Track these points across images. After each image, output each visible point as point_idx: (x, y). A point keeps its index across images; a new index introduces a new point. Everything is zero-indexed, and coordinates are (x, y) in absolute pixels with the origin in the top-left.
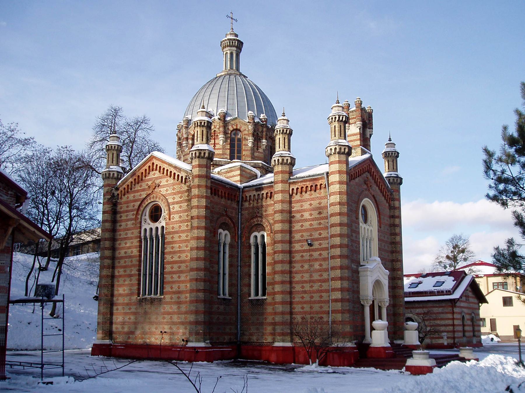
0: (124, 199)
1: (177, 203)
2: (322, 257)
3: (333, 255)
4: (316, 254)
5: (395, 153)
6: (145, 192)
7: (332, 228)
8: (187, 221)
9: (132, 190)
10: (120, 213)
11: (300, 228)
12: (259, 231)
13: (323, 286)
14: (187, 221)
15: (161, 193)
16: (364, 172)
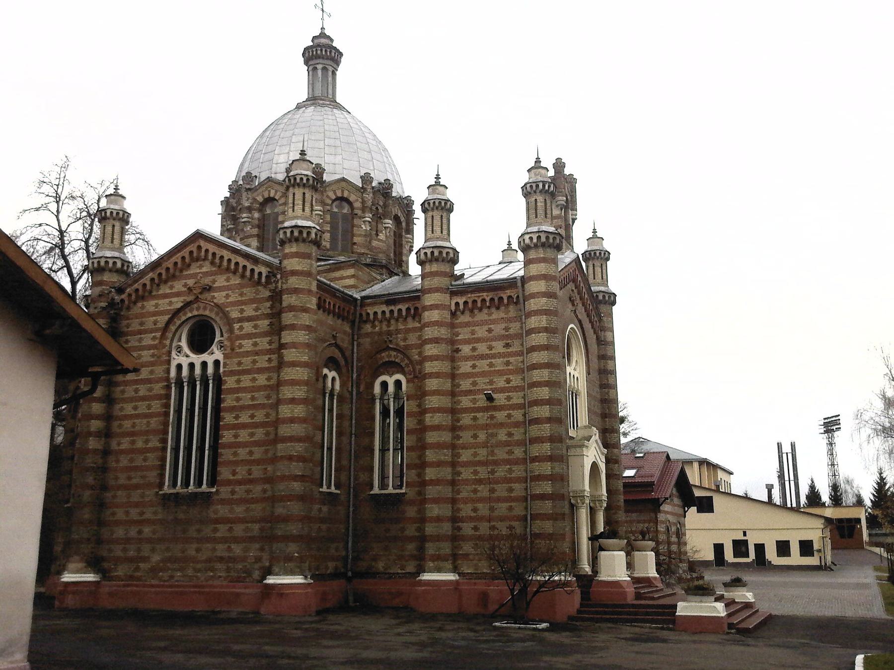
0: (136, 309)
1: (249, 319)
2: (512, 419)
3: (536, 417)
4: (501, 416)
5: (605, 253)
6: (182, 299)
7: (535, 371)
8: (270, 352)
9: (153, 294)
10: (127, 334)
11: (469, 370)
12: (391, 373)
13: (514, 470)
14: (270, 352)
15: (215, 301)
16: (555, 280)
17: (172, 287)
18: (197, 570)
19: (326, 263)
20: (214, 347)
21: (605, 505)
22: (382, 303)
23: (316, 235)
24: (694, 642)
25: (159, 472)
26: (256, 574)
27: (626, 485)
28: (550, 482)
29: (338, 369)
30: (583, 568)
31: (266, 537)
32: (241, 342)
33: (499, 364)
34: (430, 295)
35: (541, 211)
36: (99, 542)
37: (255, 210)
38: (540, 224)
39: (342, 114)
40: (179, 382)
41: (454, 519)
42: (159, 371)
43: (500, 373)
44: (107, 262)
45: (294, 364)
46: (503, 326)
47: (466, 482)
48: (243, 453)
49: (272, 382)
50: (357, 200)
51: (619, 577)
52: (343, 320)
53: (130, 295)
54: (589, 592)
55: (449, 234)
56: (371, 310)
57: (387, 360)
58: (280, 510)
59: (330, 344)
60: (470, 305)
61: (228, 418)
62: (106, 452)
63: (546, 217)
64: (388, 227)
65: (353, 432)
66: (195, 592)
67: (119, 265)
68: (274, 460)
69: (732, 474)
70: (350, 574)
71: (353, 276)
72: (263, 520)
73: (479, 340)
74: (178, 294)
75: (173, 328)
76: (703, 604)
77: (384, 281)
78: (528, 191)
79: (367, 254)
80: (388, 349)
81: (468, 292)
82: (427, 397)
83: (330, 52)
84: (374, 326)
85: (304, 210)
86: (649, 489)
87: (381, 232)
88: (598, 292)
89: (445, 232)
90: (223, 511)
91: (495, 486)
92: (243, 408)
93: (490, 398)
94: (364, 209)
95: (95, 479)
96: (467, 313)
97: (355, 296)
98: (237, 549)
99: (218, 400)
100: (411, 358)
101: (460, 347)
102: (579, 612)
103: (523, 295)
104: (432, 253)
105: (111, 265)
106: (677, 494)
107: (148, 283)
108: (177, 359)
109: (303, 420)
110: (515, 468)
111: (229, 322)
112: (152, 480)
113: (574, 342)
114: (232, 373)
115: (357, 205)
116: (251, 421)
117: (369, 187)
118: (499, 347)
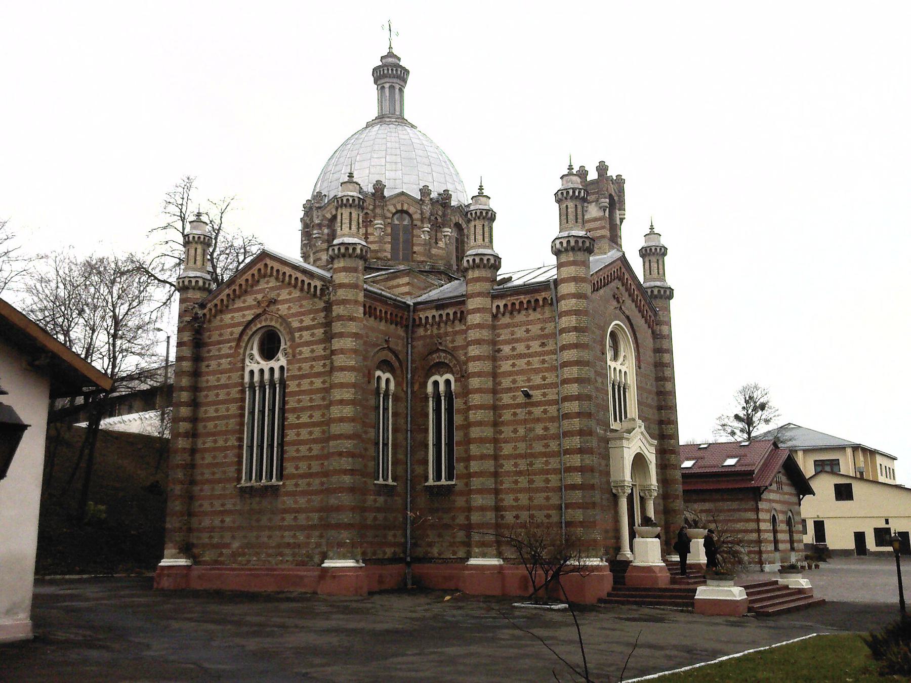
0: (216, 322)
1: (308, 328)
4: (537, 411)
5: (661, 249)
6: (252, 312)
7: (565, 368)
9: (230, 308)
17: (244, 302)
18: (269, 555)
19: (386, 272)
20: (280, 355)
21: (656, 494)
22: (431, 309)
23: (361, 250)
24: (690, 623)
25: (236, 467)
26: (317, 559)
27: (685, 476)
28: (580, 473)
29: (392, 370)
30: (625, 555)
31: (325, 525)
32: (301, 349)
33: (536, 362)
34: (472, 299)
35: (571, 217)
36: (190, 530)
37: (325, 226)
38: (571, 228)
39: (406, 130)
40: (252, 386)
41: (498, 509)
42: (235, 377)
43: (536, 371)
44: (190, 282)
45: (342, 369)
46: (539, 326)
47: (508, 473)
48: (303, 449)
49: (327, 385)
50: (416, 212)
51: (652, 562)
52: (396, 325)
53: (211, 310)
54: (624, 577)
55: (491, 241)
56: (422, 315)
57: (443, 360)
58: (333, 501)
59: (382, 348)
60: (509, 307)
61: (291, 418)
62: (193, 451)
63: (577, 222)
64: (447, 236)
65: (409, 429)
66: (267, 575)
67: (201, 283)
68: (327, 457)
69: (895, 459)
70: (408, 559)
71: (408, 284)
72: (320, 510)
73: (517, 340)
74: (249, 308)
75: (246, 338)
76: (721, 588)
77: (442, 286)
78: (561, 197)
79: (426, 262)
80: (438, 350)
81: (507, 296)
82: (470, 396)
83: (397, 70)
84: (426, 330)
85: (350, 228)
86: (749, 477)
87: (441, 240)
88: (652, 287)
89: (487, 240)
90: (289, 502)
91: (534, 477)
92: (303, 409)
93: (527, 395)
94: (422, 220)
95: (185, 475)
96: (507, 315)
97: (408, 302)
98: (301, 537)
99: (284, 403)
100: (458, 358)
101: (502, 347)
102: (609, 595)
103: (556, 296)
104: (474, 260)
105: (193, 284)
106: (787, 482)
107: (225, 298)
108: (250, 366)
109: (352, 420)
110: (551, 460)
111: (291, 332)
112: (231, 475)
113: (621, 336)
114: (294, 377)
115: (417, 216)
116: (309, 421)
117: (426, 199)
118: (535, 346)
